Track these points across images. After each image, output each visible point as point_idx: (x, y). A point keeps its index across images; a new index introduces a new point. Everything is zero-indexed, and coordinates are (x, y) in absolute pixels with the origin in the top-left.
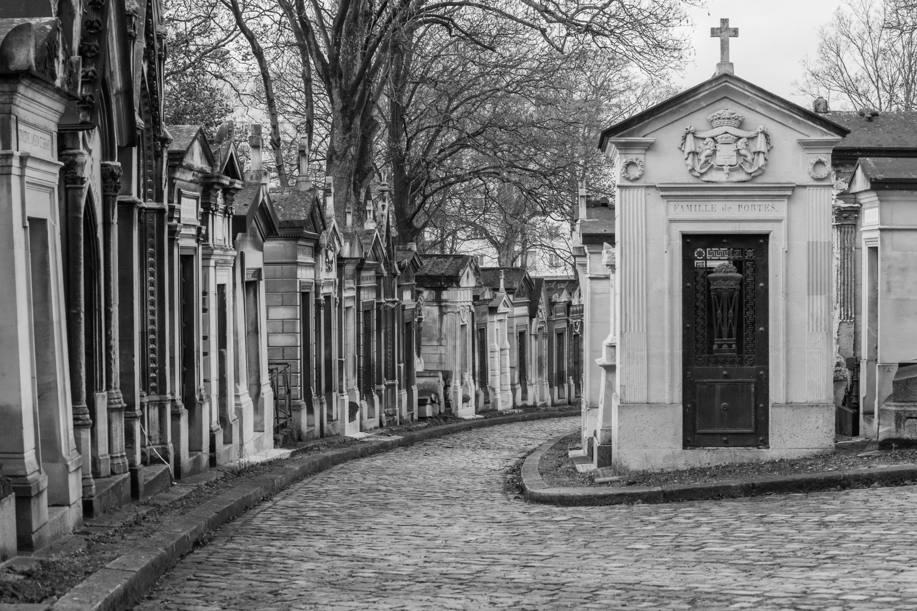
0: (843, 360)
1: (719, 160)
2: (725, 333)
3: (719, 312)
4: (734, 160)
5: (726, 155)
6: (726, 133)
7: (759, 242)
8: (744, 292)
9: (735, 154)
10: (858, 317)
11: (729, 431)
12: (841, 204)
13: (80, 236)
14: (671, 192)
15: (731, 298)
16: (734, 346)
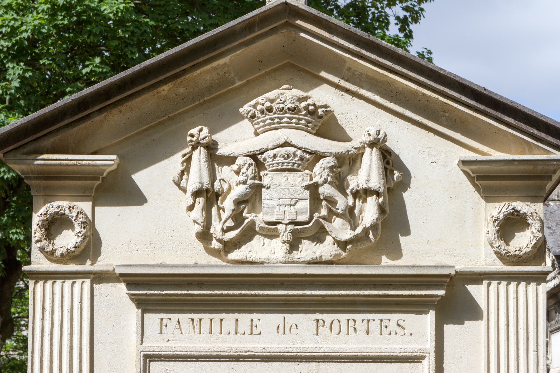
1: (269, 211)
6: (286, 144)
9: (306, 194)
13: (163, 291)
14: (157, 292)
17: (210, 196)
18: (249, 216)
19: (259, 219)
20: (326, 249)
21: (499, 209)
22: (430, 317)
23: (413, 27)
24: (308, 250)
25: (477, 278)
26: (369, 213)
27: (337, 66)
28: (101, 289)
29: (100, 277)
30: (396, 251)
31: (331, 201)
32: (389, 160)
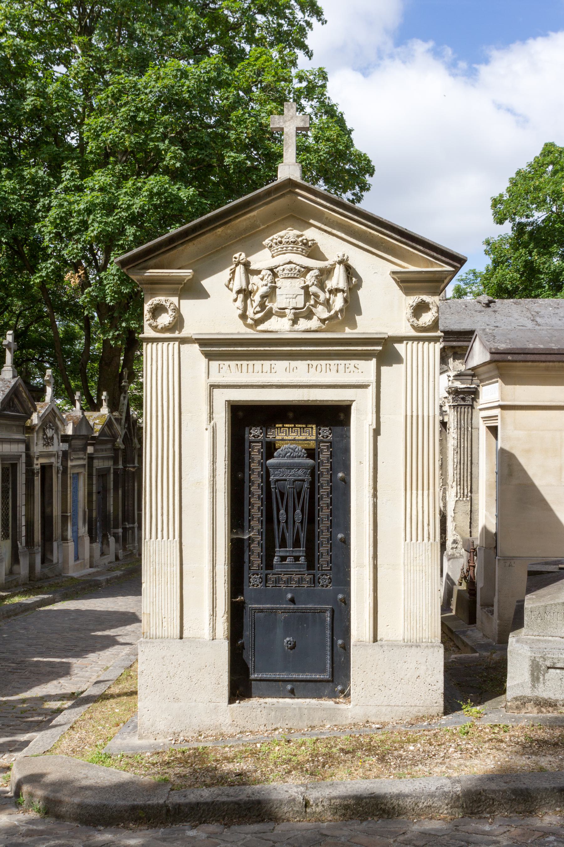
0: (459, 538)
2: (290, 541)
3: (282, 511)
4: (300, 302)
5: (289, 294)
6: (290, 263)
7: (335, 416)
8: (317, 484)
9: (302, 292)
10: (473, 495)
11: (295, 676)
12: (458, 384)
14: (217, 349)
15: (299, 494)
16: (302, 559)
17: (246, 293)
18: (269, 305)
20: (314, 323)
21: (414, 300)
22: (374, 362)
24: (303, 324)
25: (400, 340)
26: (338, 302)
27: (320, 217)
28: (184, 347)
30: (354, 325)
31: (316, 296)
32: (350, 271)
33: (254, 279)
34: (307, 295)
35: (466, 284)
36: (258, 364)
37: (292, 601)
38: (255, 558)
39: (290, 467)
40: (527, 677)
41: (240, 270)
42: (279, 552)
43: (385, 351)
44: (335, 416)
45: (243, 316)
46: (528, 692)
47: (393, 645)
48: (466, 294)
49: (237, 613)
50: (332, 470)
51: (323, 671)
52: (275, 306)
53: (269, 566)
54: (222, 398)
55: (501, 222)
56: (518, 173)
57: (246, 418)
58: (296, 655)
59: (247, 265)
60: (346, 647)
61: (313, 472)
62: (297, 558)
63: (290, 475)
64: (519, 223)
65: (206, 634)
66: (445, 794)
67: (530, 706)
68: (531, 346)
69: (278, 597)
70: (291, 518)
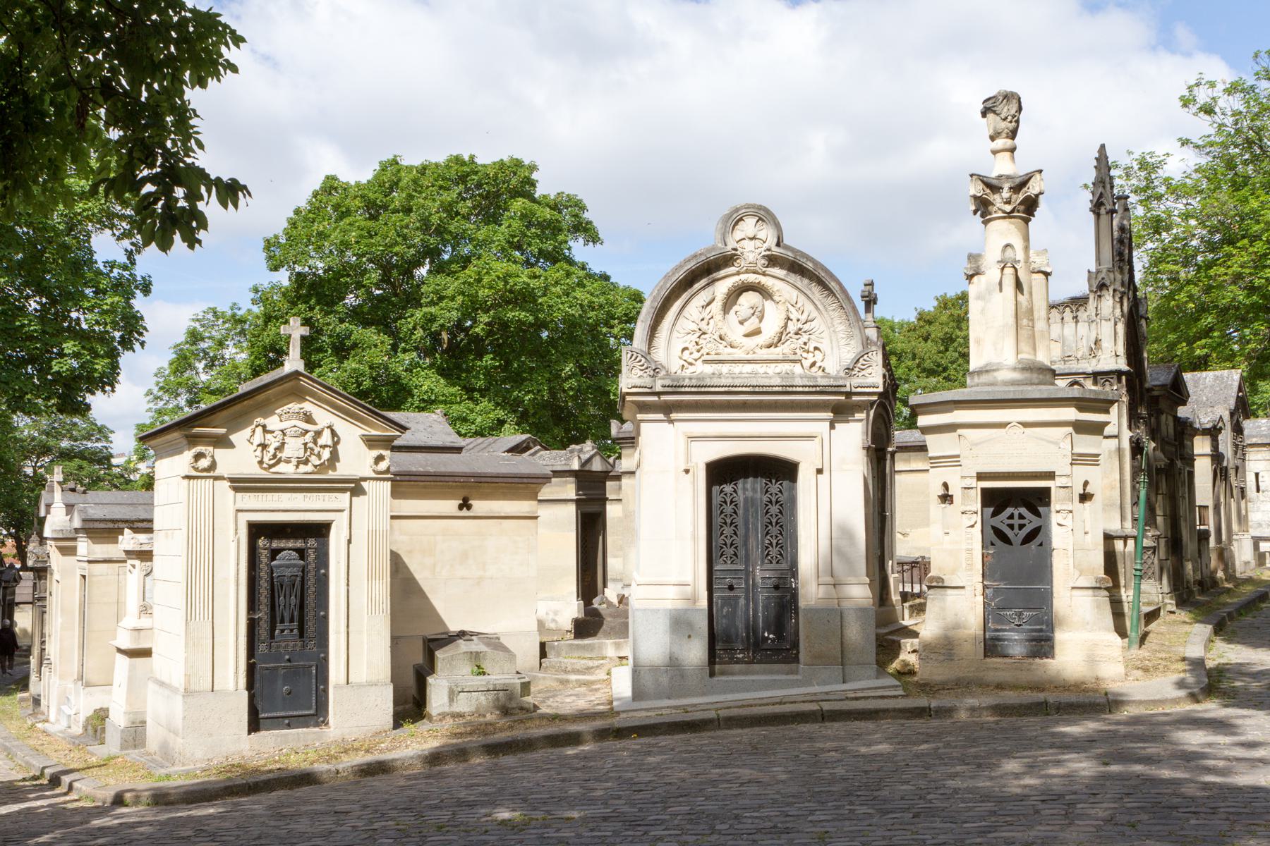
2: (287, 619)
5: (294, 448)
7: (320, 531)
14: (241, 485)
17: (264, 446)
18: (279, 455)
19: (284, 455)
20: (309, 468)
21: (375, 453)
22: (348, 494)
23: (137, 257)
24: (303, 468)
25: (365, 479)
26: (326, 454)
27: (313, 395)
28: (217, 483)
29: (216, 478)
30: (334, 469)
31: (312, 449)
32: (334, 434)
33: (269, 436)
34: (306, 449)
35: (203, 326)
36: (269, 495)
37: (289, 660)
38: (263, 632)
39: (288, 566)
40: (445, 699)
41: (259, 430)
42: (279, 626)
43: (355, 487)
44: (320, 531)
45: (261, 462)
46: (447, 709)
47: (360, 686)
48: (202, 339)
49: (251, 670)
50: (317, 568)
51: (310, 708)
52: (284, 455)
53: (272, 636)
54: (245, 518)
55: (275, 268)
56: (297, 212)
57: (257, 531)
58: (292, 699)
59: (264, 427)
60: (326, 691)
61: (304, 570)
62: (292, 630)
63: (287, 573)
64: (299, 274)
65: (231, 686)
66: (419, 756)
67: (448, 718)
68: (414, 469)
69: (278, 658)
70: (288, 602)
